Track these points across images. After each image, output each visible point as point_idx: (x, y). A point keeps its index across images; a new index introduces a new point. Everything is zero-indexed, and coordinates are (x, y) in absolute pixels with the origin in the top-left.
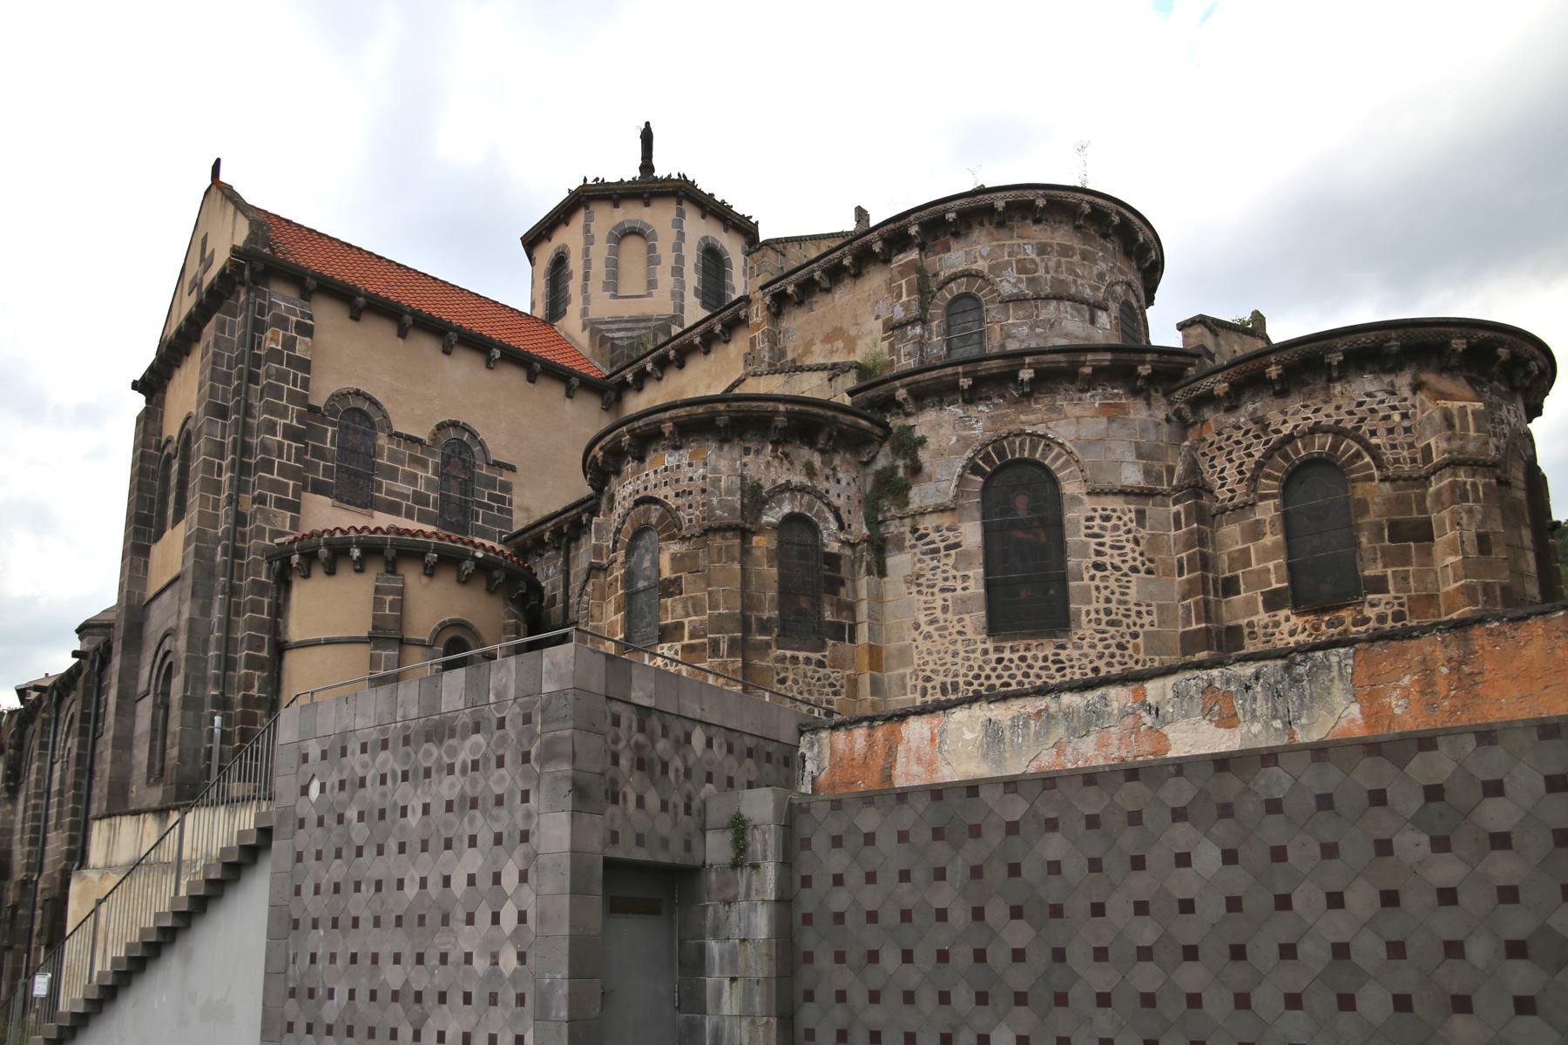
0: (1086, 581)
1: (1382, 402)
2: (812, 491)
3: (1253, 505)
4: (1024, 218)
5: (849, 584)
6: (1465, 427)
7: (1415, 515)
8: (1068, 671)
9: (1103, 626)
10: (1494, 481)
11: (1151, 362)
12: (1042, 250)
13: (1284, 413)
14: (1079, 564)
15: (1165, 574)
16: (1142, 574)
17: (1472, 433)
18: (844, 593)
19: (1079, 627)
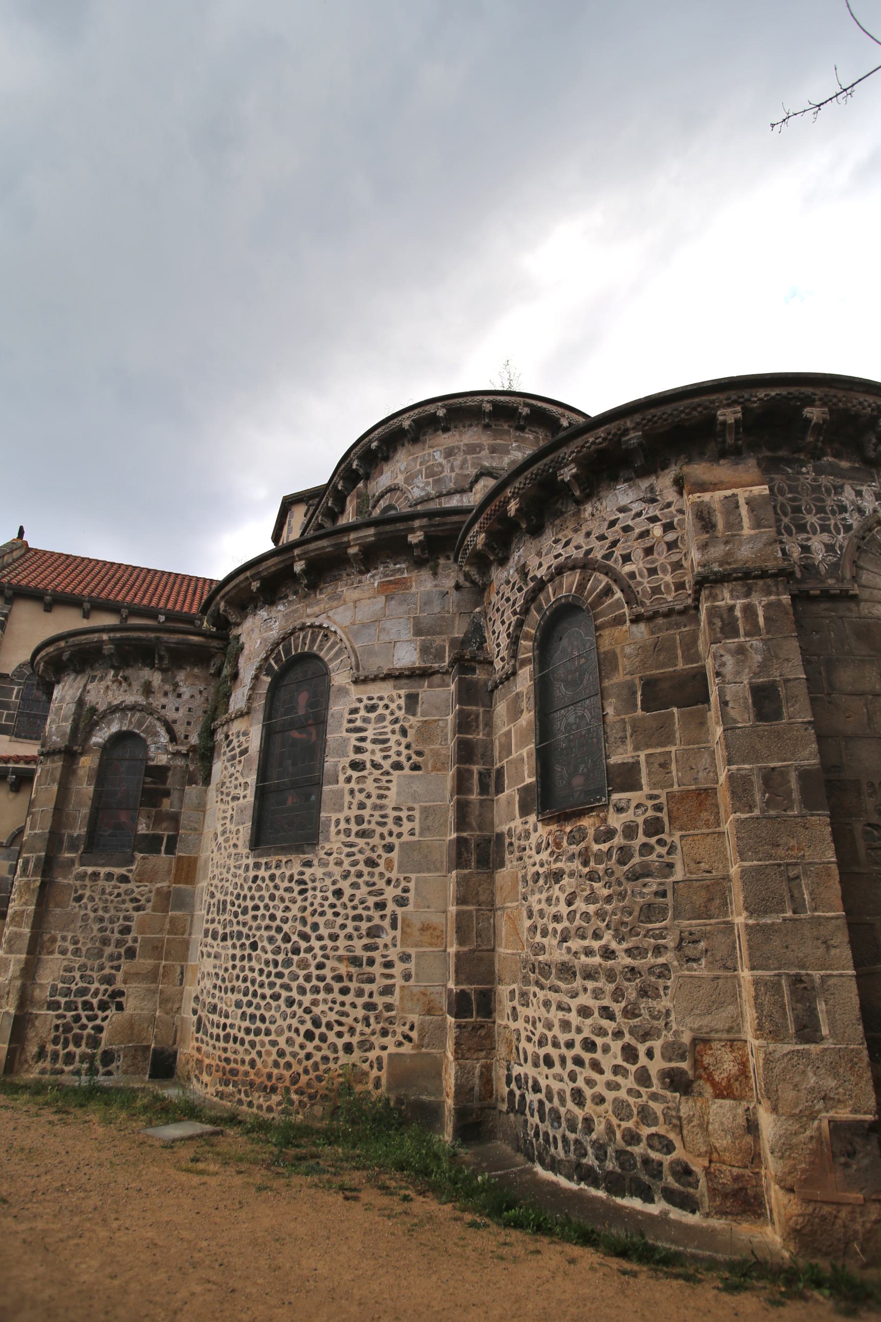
0: (342, 784)
1: (639, 514)
2: (148, 710)
3: (514, 673)
4: (436, 431)
5: (175, 795)
6: (734, 524)
7: (681, 666)
8: (310, 894)
9: (352, 839)
10: (786, 598)
11: (421, 528)
12: (449, 453)
13: (539, 554)
14: (336, 765)
15: (435, 768)
16: (407, 771)
17: (747, 530)
18: (167, 805)
19: (327, 839)
